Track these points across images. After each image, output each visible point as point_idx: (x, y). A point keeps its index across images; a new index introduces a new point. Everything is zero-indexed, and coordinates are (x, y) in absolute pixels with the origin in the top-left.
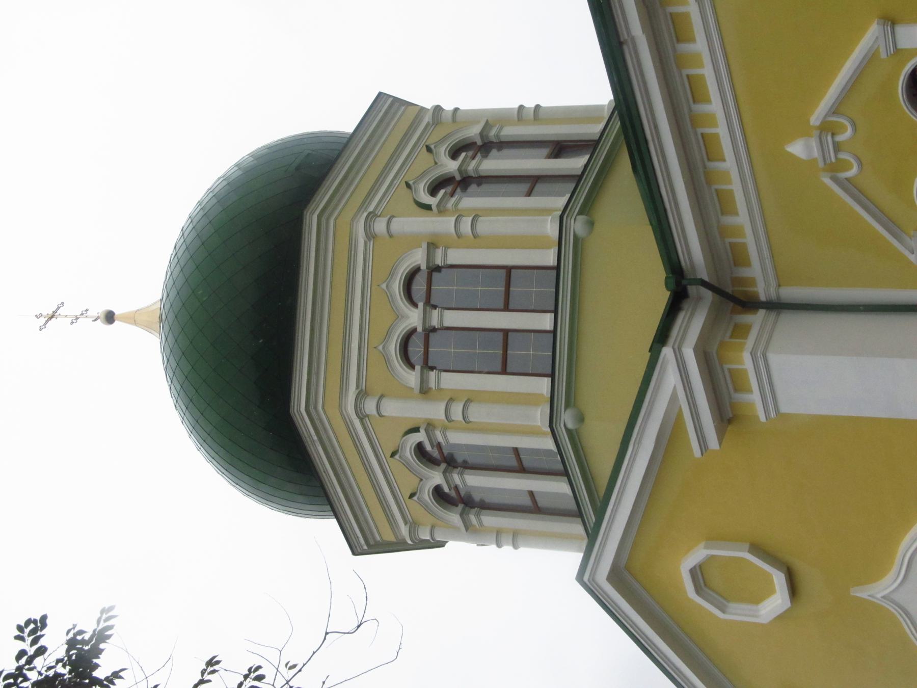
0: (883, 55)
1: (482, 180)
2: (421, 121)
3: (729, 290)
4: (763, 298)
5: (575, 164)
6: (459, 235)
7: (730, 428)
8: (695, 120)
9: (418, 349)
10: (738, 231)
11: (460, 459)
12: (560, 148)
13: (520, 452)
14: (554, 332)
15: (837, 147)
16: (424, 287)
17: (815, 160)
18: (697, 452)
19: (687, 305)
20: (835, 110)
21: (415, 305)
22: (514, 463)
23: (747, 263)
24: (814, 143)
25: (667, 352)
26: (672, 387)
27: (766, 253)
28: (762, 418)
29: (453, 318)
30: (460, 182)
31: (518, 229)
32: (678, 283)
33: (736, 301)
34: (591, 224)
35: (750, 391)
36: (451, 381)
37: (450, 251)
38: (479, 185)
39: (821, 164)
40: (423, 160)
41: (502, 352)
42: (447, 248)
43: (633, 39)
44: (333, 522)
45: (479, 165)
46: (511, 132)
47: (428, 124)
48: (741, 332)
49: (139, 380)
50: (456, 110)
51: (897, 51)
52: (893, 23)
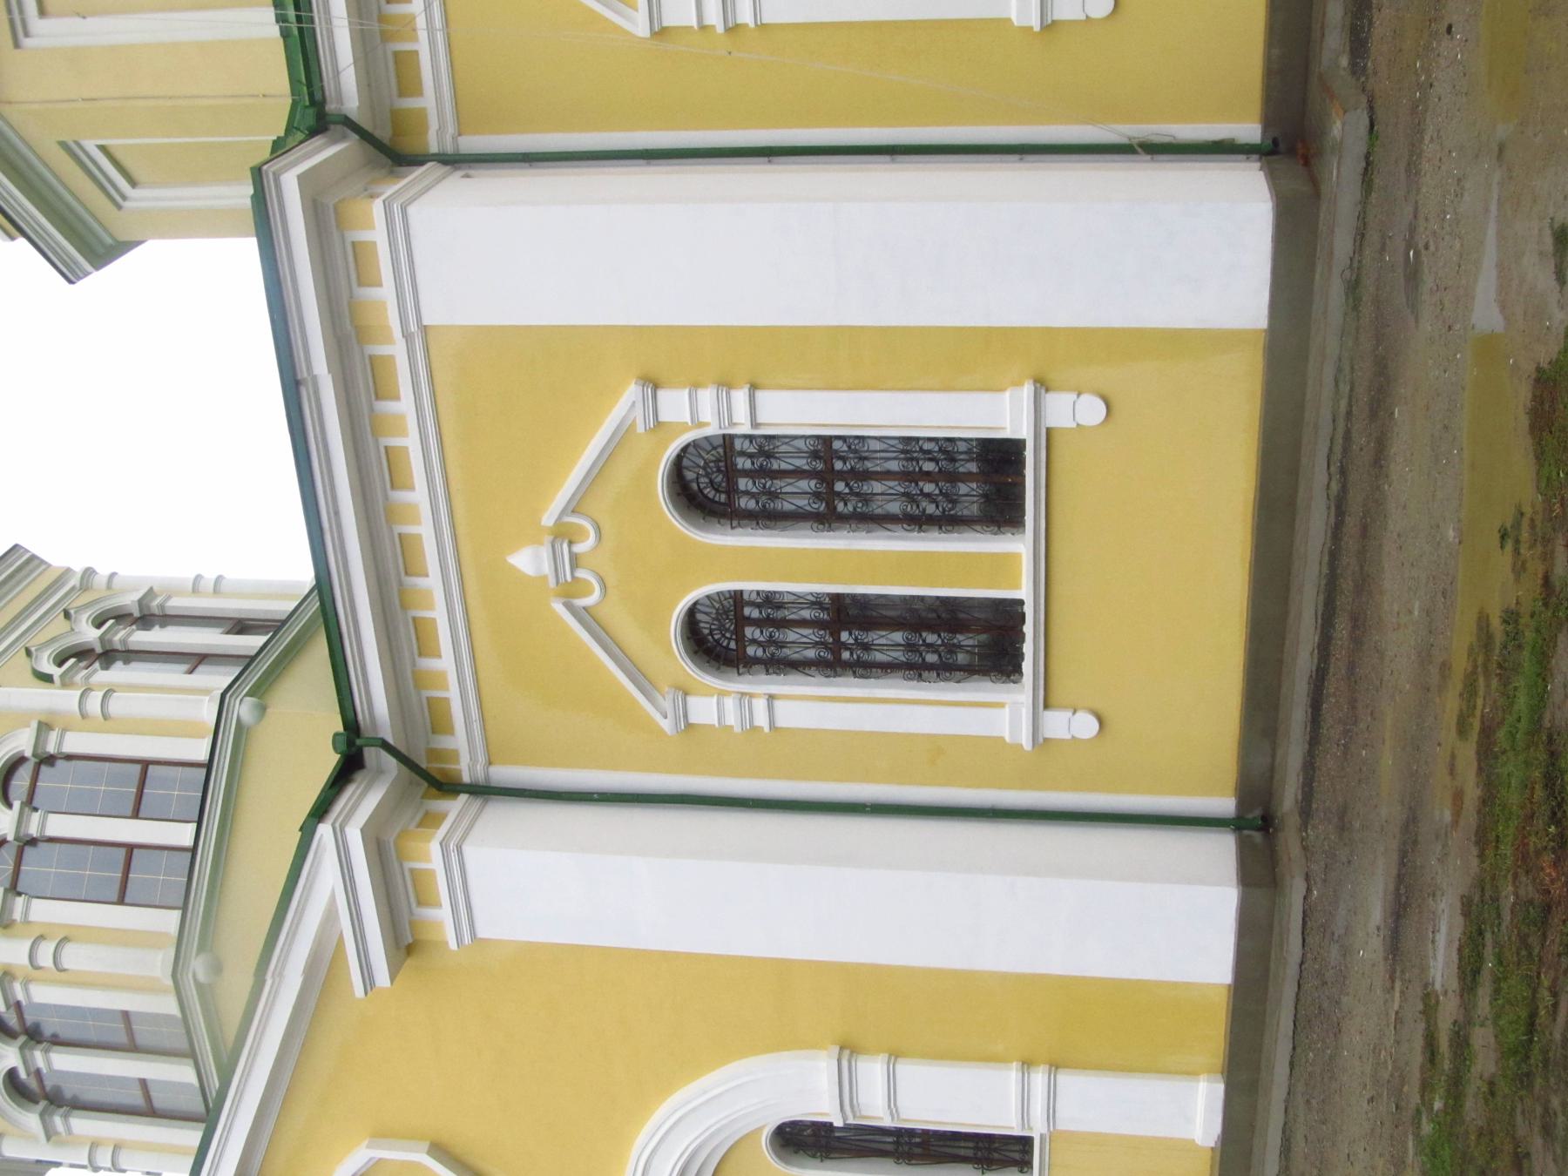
0: (640, 429)
2: (63, 585)
3: (424, 765)
4: (466, 779)
5: (254, 642)
6: (84, 716)
7: (409, 962)
8: (392, 514)
10: (439, 679)
11: (48, 1031)
12: (241, 626)
13: (133, 1019)
14: (194, 850)
15: (575, 561)
16: (27, 783)
17: (545, 577)
18: (359, 991)
19: (359, 777)
20: (575, 506)
21: (10, 806)
22: (122, 1038)
23: (449, 730)
24: (545, 553)
25: (324, 830)
26: (328, 893)
27: (476, 727)
28: (453, 945)
30: (99, 656)
31: (162, 713)
32: (350, 743)
33: (434, 781)
34: (262, 709)
35: (439, 905)
36: (44, 911)
37: (69, 735)
38: (127, 662)
39: (552, 582)
40: (59, 625)
41: (123, 876)
42: (64, 730)
43: (315, 379)
45: (129, 635)
46: (177, 604)
47: (73, 588)
48: (431, 820)
50: (113, 575)
51: (658, 424)
52: (656, 387)
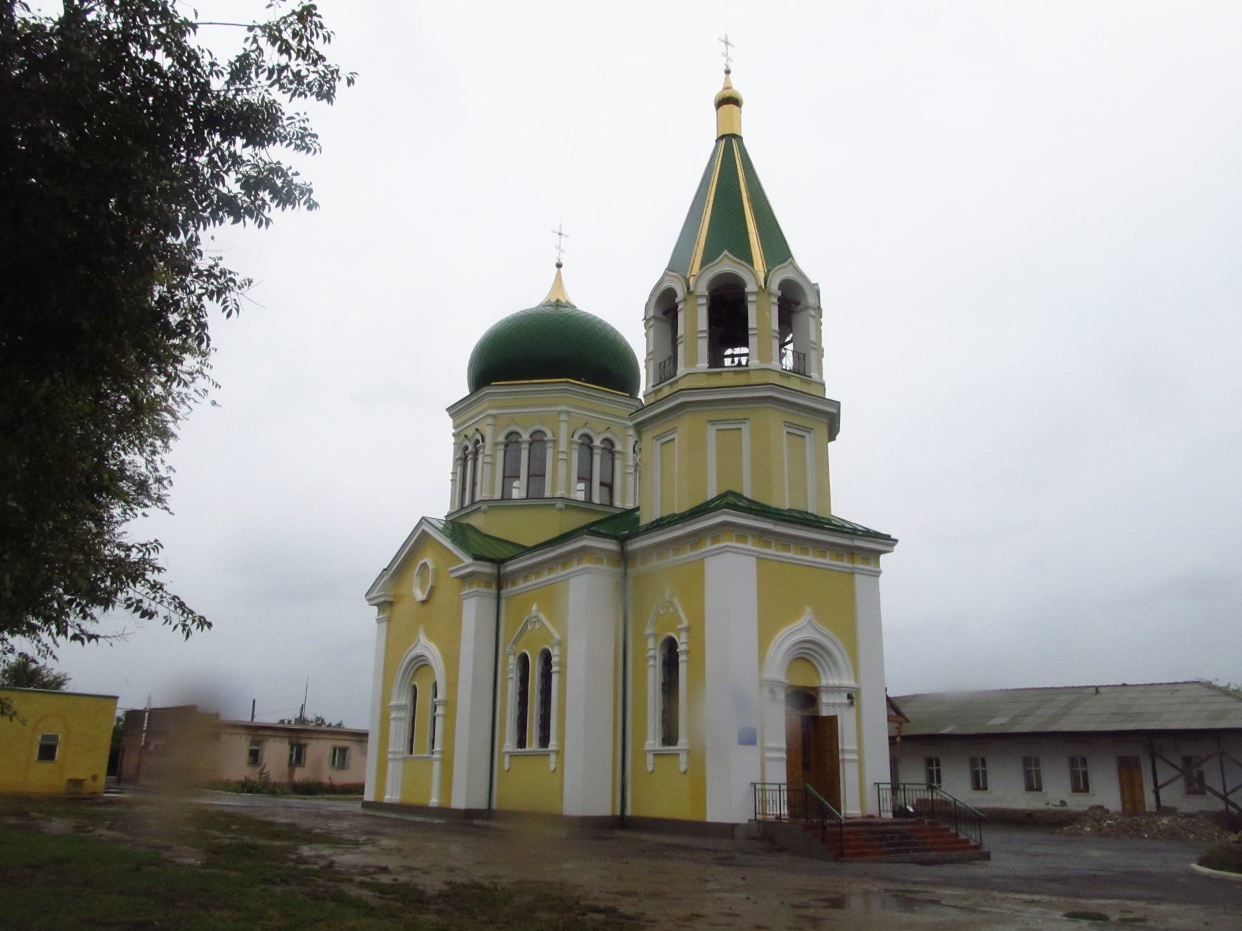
1: (592, 455)
9: (512, 440)
29: (524, 455)
33: (500, 582)
44: (467, 393)
48: (488, 585)
49: (527, 297)
